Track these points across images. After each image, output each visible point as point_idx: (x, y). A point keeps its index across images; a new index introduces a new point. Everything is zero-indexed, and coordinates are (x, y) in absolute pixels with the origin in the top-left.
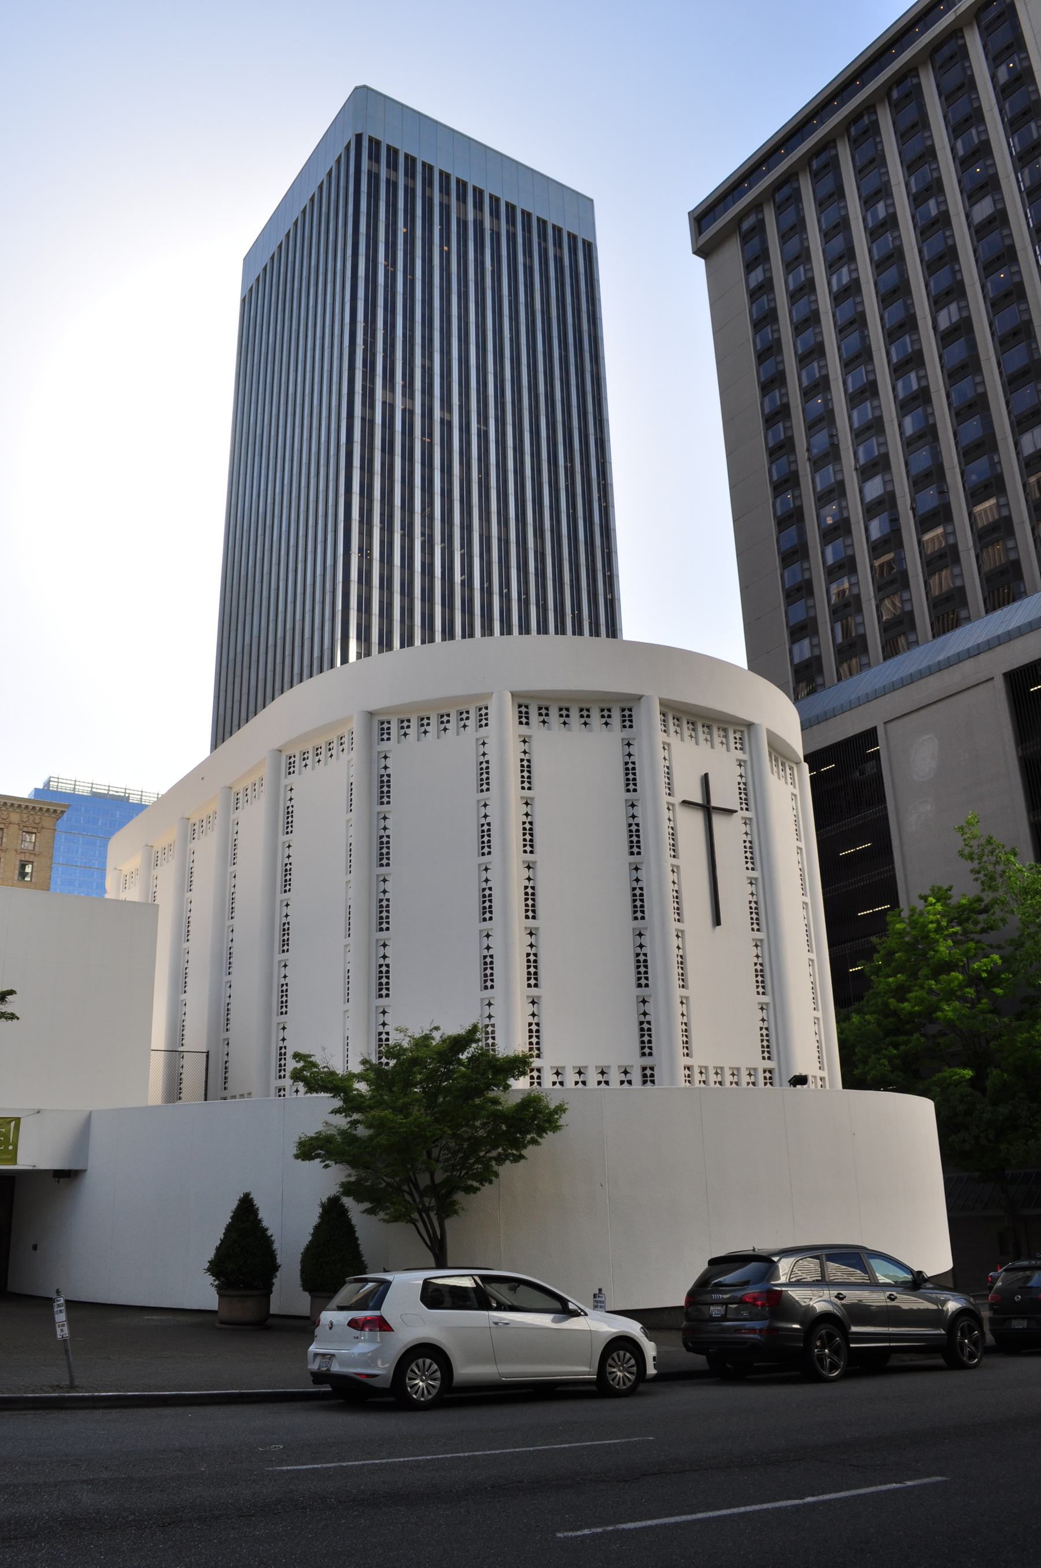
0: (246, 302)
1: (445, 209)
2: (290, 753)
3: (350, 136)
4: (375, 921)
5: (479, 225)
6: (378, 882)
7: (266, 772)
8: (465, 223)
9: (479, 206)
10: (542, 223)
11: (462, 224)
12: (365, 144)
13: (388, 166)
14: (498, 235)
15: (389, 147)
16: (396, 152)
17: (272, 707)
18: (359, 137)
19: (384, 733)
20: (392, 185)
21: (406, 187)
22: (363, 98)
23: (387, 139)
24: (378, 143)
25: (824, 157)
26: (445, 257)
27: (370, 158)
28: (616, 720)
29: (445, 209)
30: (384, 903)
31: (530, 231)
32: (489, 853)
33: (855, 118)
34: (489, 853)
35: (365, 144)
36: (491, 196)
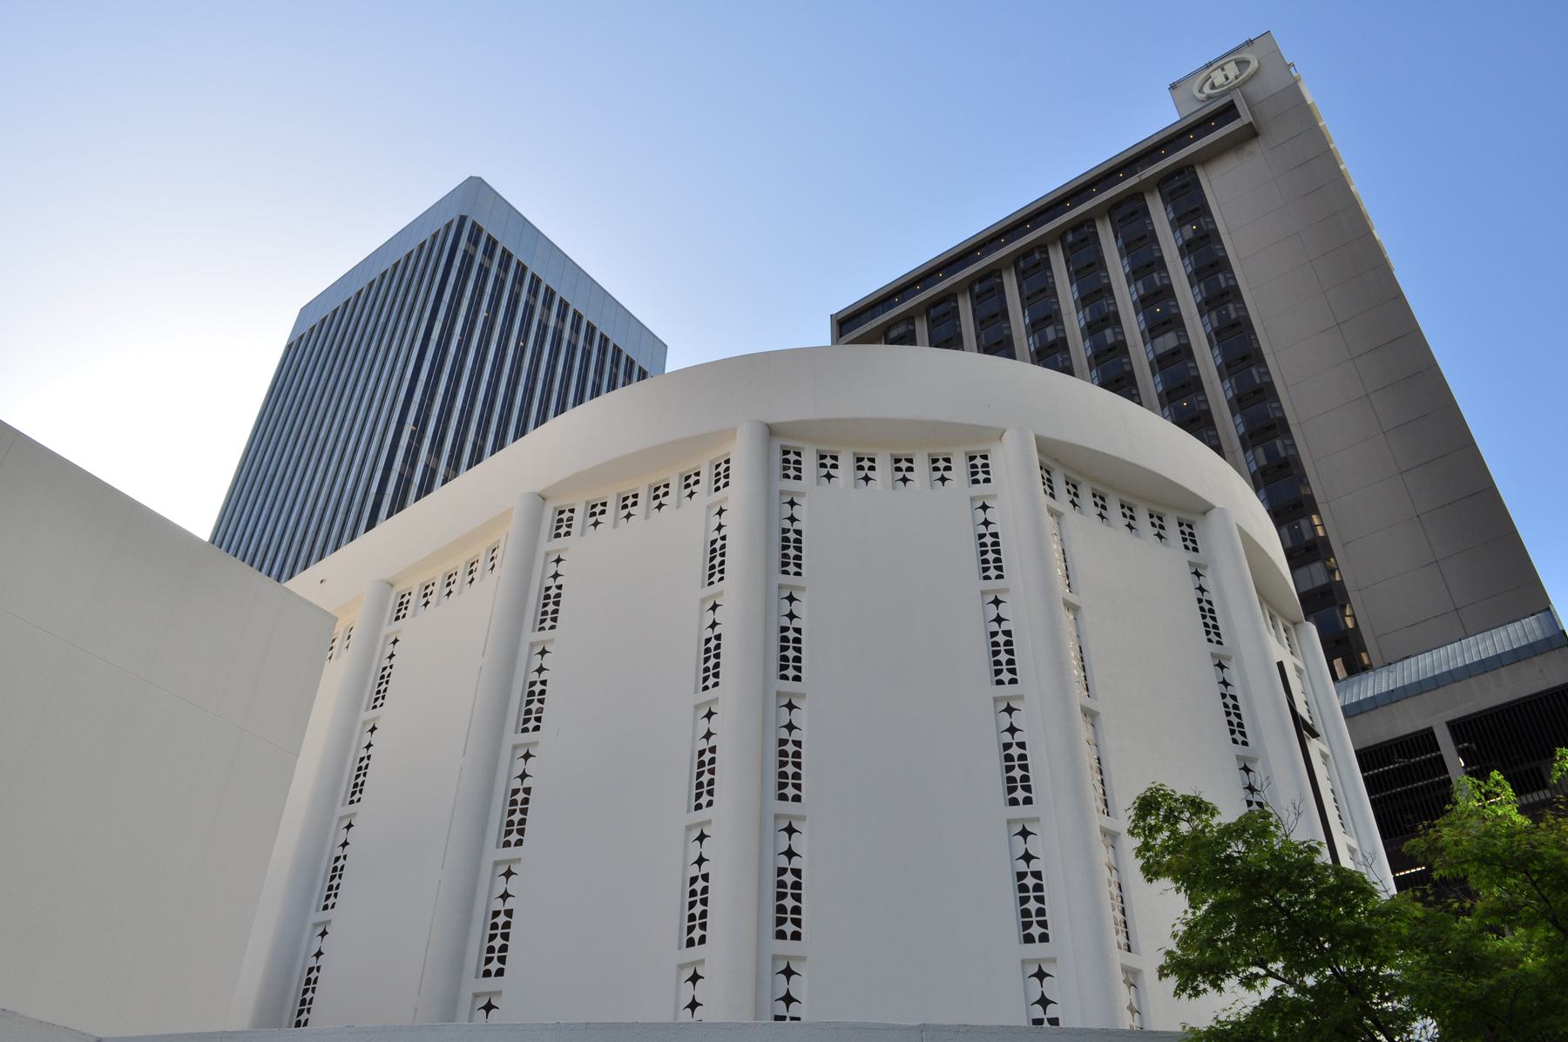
0: (293, 349)
1: (529, 309)
2: (565, 503)
3: (454, 215)
4: (773, 780)
5: (558, 334)
6: (998, 712)
7: (509, 538)
8: (546, 327)
9: (562, 316)
10: (618, 351)
11: (543, 327)
12: (468, 226)
13: (485, 253)
14: (575, 348)
15: (489, 237)
16: (495, 243)
17: (555, 424)
18: (463, 219)
19: (790, 464)
20: (484, 272)
21: (497, 277)
22: (476, 188)
23: (489, 229)
24: (480, 230)
25: (987, 284)
26: (520, 352)
27: (469, 239)
28: (1173, 531)
29: (529, 309)
30: (790, 748)
31: (604, 355)
32: (500, 972)
33: (1026, 253)
34: (500, 972)
35: (468, 226)
36: (575, 312)
